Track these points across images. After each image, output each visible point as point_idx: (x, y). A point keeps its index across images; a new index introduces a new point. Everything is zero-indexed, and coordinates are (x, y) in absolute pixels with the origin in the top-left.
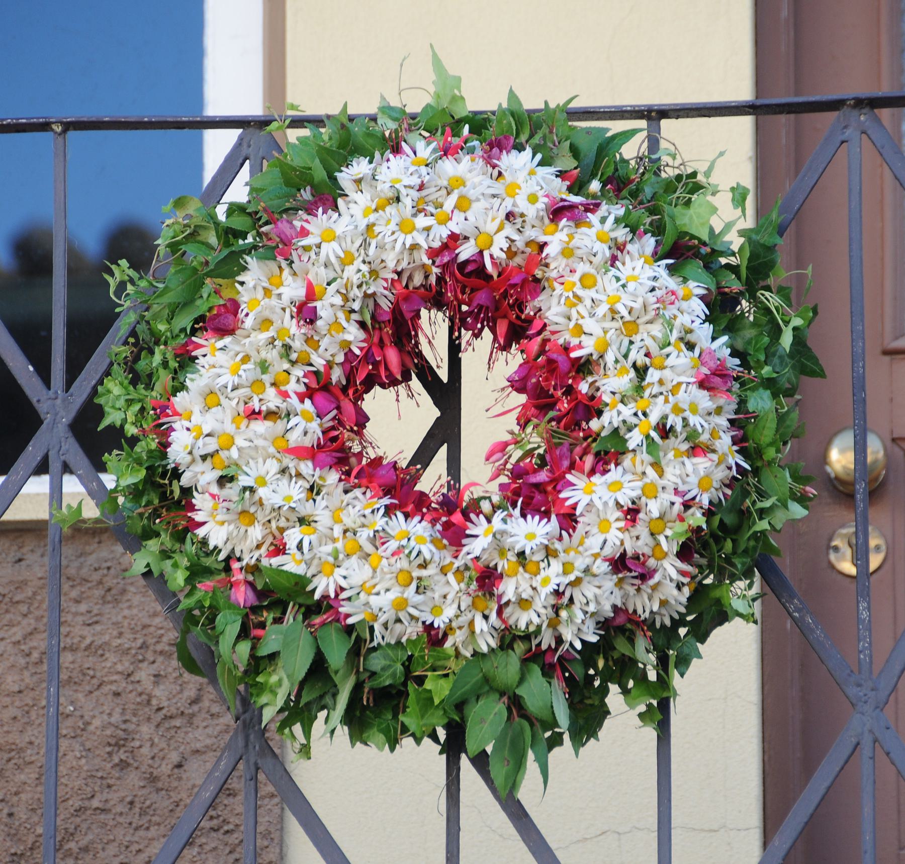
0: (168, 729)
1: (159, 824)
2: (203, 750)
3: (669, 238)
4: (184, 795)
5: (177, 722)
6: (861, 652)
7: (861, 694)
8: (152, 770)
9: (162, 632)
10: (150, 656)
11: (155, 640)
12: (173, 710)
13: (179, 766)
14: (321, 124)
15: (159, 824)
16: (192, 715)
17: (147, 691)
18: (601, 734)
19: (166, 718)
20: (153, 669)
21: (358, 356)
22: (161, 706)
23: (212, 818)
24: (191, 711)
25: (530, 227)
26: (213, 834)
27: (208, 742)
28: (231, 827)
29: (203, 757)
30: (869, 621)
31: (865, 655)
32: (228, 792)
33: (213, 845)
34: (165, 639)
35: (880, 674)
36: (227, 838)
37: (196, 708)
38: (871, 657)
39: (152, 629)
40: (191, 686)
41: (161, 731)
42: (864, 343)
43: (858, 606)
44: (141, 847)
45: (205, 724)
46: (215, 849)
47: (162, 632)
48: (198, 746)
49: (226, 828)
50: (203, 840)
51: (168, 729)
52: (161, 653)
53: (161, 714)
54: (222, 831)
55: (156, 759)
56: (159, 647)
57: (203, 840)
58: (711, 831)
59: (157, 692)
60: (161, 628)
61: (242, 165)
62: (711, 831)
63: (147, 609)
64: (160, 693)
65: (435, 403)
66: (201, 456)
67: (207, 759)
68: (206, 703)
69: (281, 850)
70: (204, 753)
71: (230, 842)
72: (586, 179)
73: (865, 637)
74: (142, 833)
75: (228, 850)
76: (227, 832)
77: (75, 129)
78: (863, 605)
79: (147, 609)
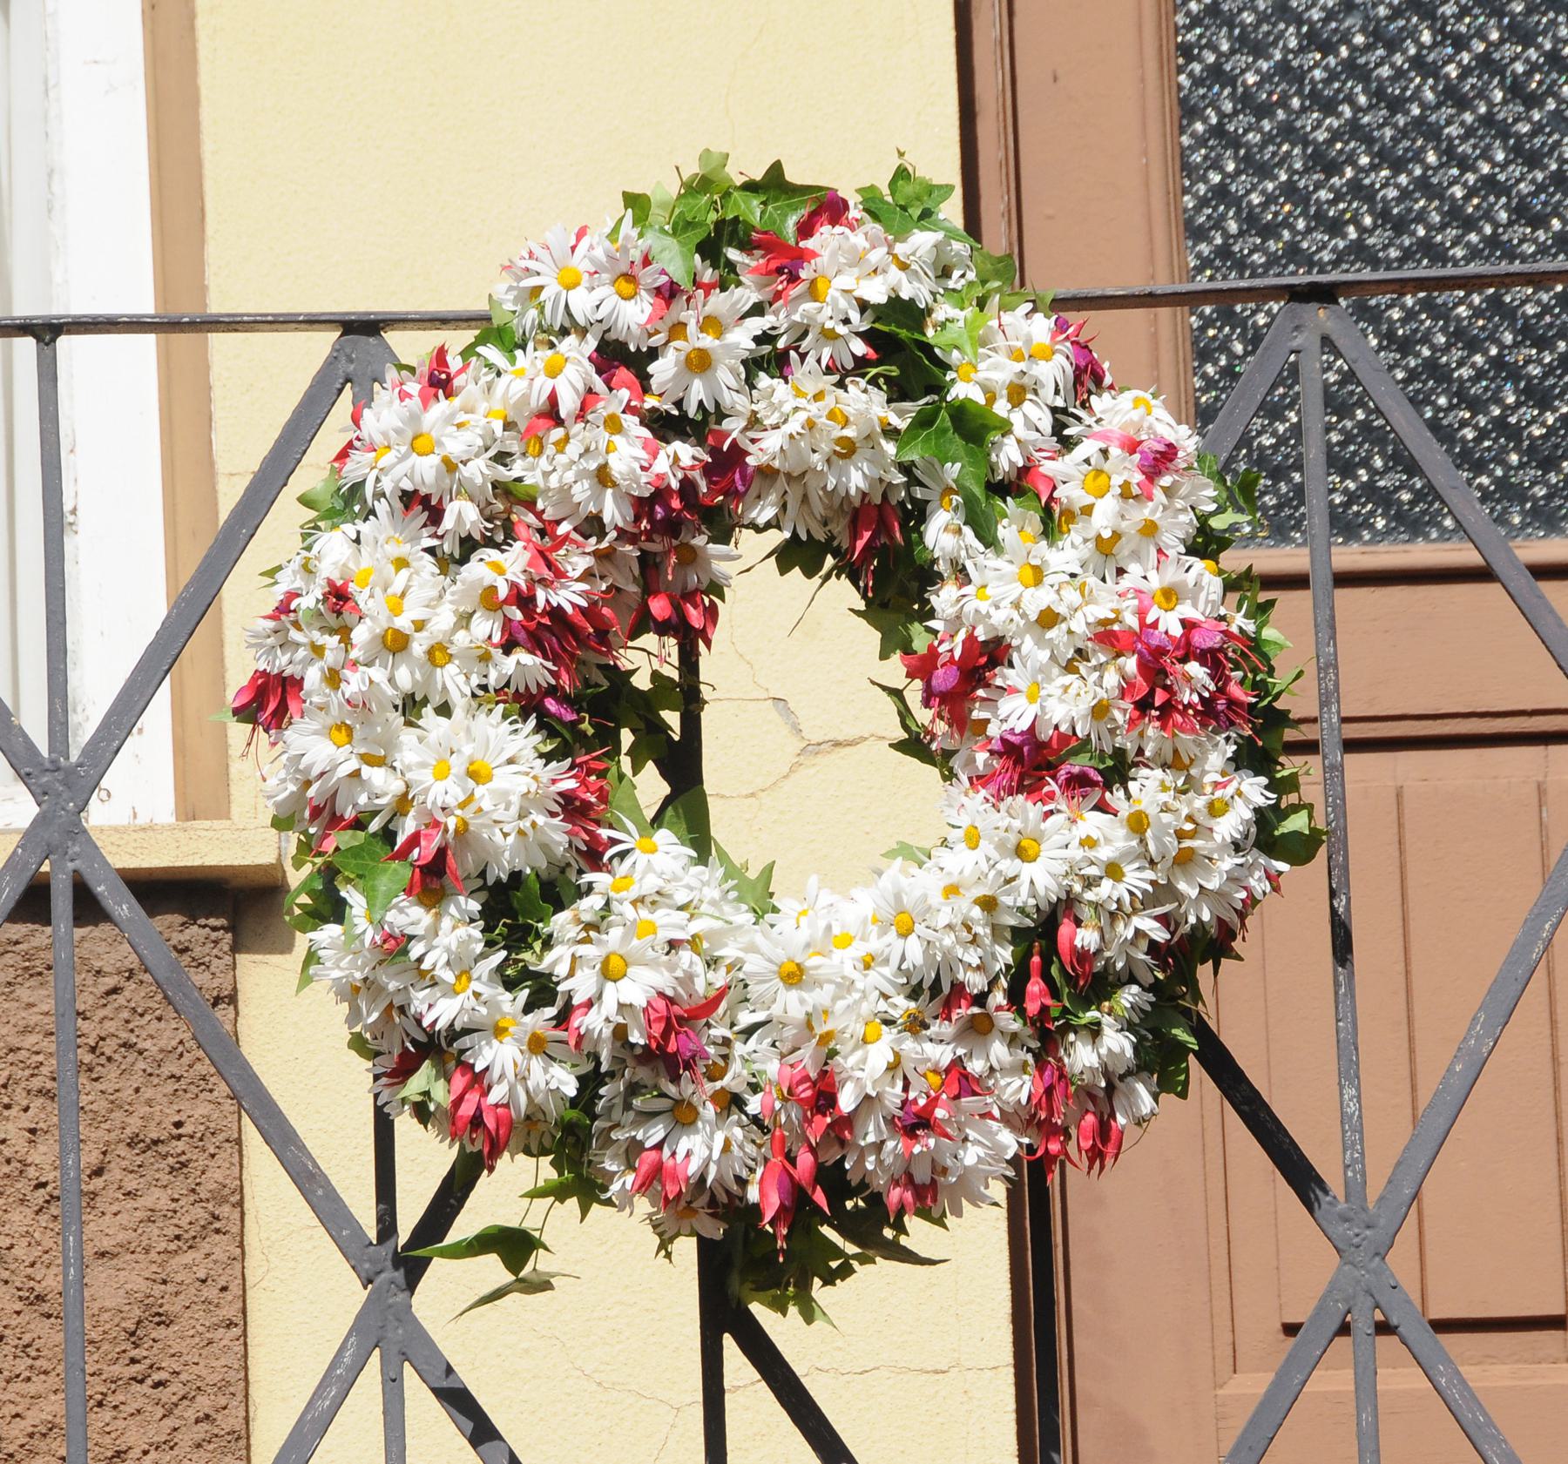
1: (46, 1373)
2: (116, 1250)
3: (1160, 598)
6: (1347, 1167)
7: (1350, 1233)
8: (32, 1284)
9: (40, 1058)
10: (21, 1098)
11: (27, 1072)
15: (46, 1373)
16: (94, 1194)
17: (18, 1157)
18: (353, 1053)
20: (26, 1121)
22: (43, 1180)
23: (133, 1361)
24: (91, 1188)
26: (136, 1387)
27: (122, 1237)
28: (162, 1375)
29: (115, 1261)
30: (1360, 1117)
31: (1354, 1171)
32: (157, 1319)
33: (136, 1406)
34: (44, 1070)
36: (156, 1393)
37: (98, 1183)
38: (1364, 1174)
39: (23, 1054)
40: (91, 1146)
41: (44, 1219)
42: (1337, 675)
43: (1341, 1095)
44: (19, 1409)
45: (115, 1208)
47: (40, 1058)
48: (106, 1244)
49: (157, 1377)
50: (120, 1397)
54: (149, 1382)
55: (38, 1266)
56: (36, 1083)
57: (120, 1397)
58: (936, 1372)
59: (35, 1157)
60: (38, 1053)
61: (340, 391)
62: (936, 1372)
63: (13, 1021)
64: (43, 1155)
65: (662, 774)
67: (121, 1266)
68: (114, 1173)
69: (247, 1411)
70: (115, 1256)
71: (164, 1400)
73: (1353, 1143)
74: (18, 1386)
75: (160, 1412)
76: (157, 1385)
77: (69, 332)
78: (1350, 1092)
79: (13, 1021)
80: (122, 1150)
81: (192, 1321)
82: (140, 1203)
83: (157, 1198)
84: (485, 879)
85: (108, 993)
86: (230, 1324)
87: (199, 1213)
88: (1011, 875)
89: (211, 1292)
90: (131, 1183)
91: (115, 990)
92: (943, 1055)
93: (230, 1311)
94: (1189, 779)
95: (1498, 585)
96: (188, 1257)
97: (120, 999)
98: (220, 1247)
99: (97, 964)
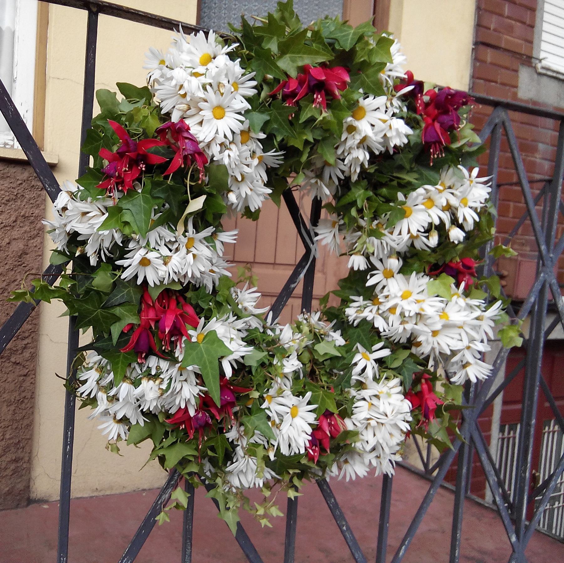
0: (5, 230)
4: (10, 253)
5: (8, 228)
12: (7, 224)
13: (9, 243)
14: (410, 187)
19: (5, 226)
21: (509, 425)
25: (198, 128)
28: (25, 265)
34: (5, 199)
35: (402, 413)
37: (15, 224)
46: (20, 272)
48: (16, 237)
51: (5, 230)
52: (3, 203)
53: (3, 225)
61: (340, 353)
66: (327, 410)
68: (18, 222)
72: (442, 233)
80: (20, 218)
81: (33, 255)
82: (23, 229)
83: (27, 228)
84: (204, 32)
85: (20, 184)
86: (40, 256)
87: (35, 232)
88: (232, 342)
89: (36, 249)
90: (21, 225)
91: (21, 184)
92: (232, 497)
93: (40, 253)
94: (420, 428)
95: (276, 207)
96: (32, 241)
97: (22, 186)
98: (38, 240)
99: (18, 178)
